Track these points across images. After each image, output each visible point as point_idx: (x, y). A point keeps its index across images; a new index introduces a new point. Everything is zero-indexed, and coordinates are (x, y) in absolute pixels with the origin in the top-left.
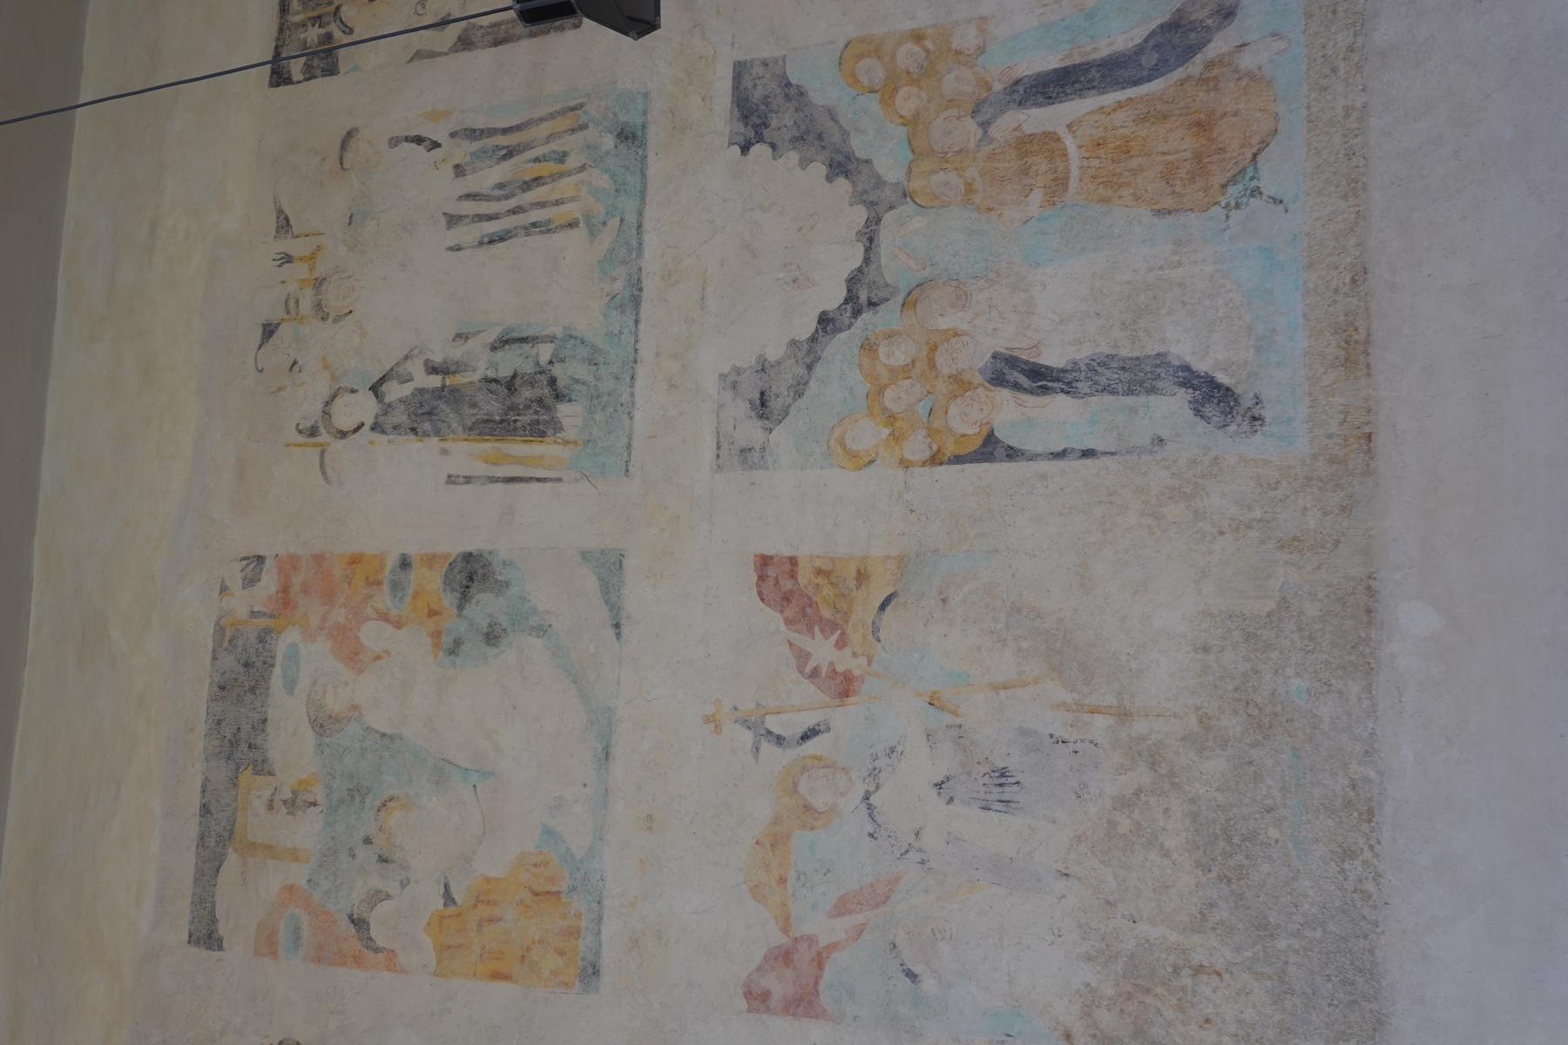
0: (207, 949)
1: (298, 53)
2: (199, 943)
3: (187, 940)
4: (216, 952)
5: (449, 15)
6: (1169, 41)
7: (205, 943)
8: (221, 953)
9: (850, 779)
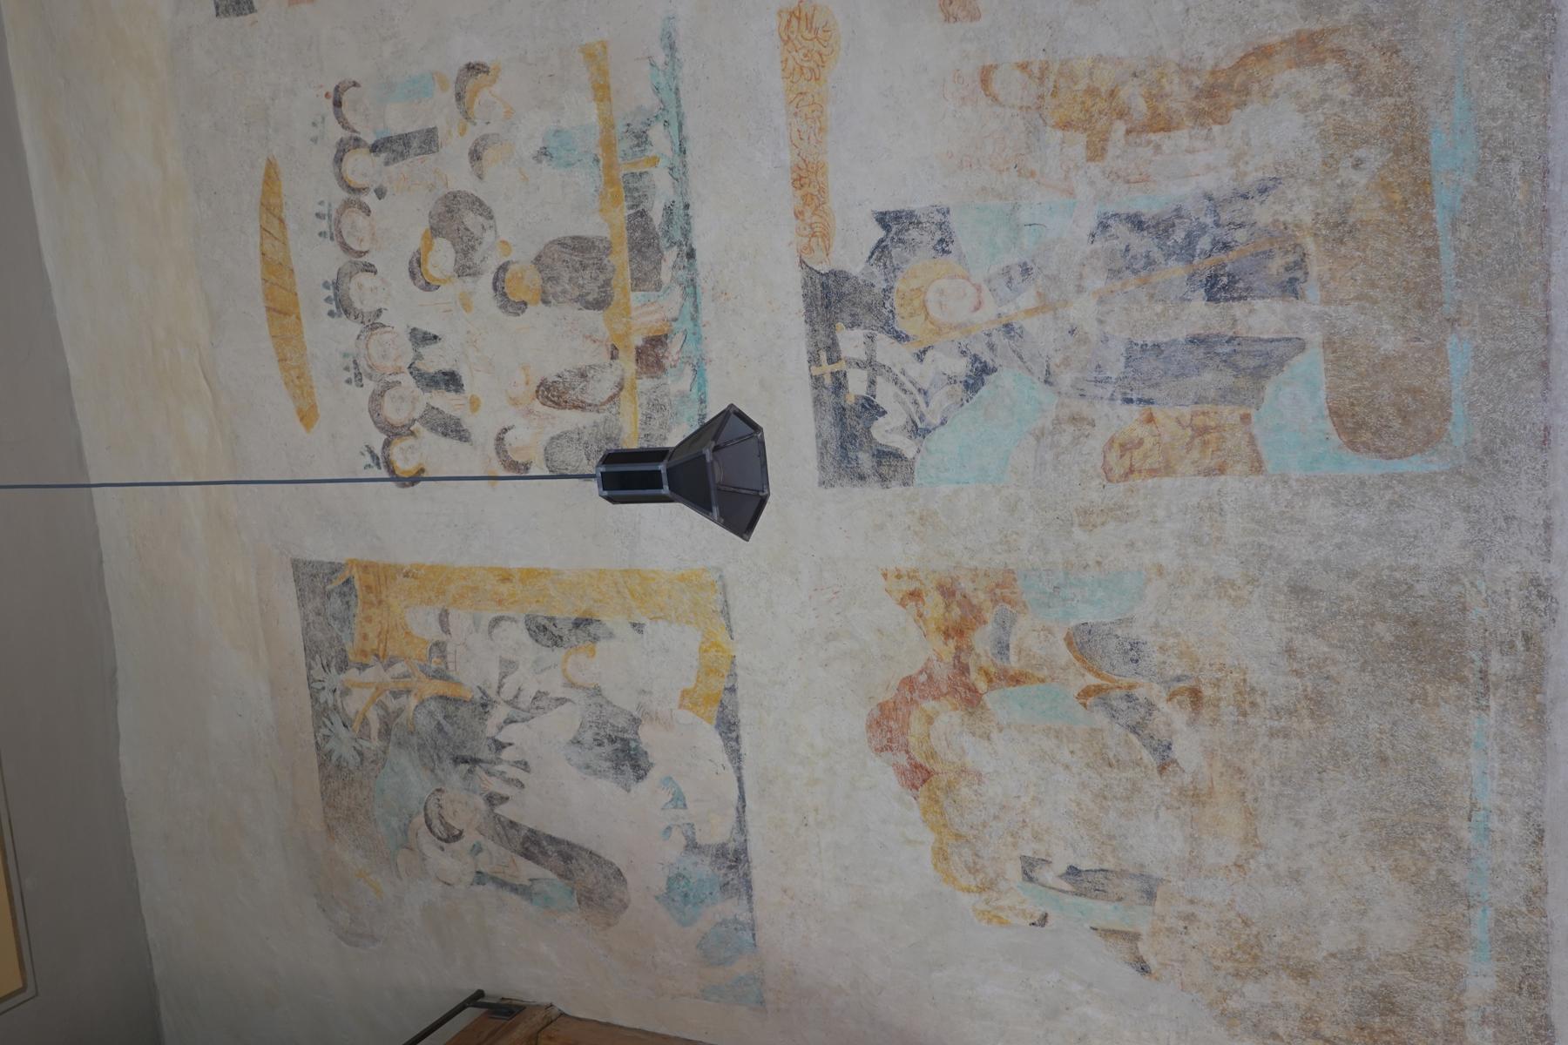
0: (238, 15)
1: (515, 475)
2: (228, 12)
3: (215, 13)
4: (249, 16)
5: (665, 260)
6: (1298, 199)
7: (234, 10)
8: (254, 15)
9: (1154, 181)
